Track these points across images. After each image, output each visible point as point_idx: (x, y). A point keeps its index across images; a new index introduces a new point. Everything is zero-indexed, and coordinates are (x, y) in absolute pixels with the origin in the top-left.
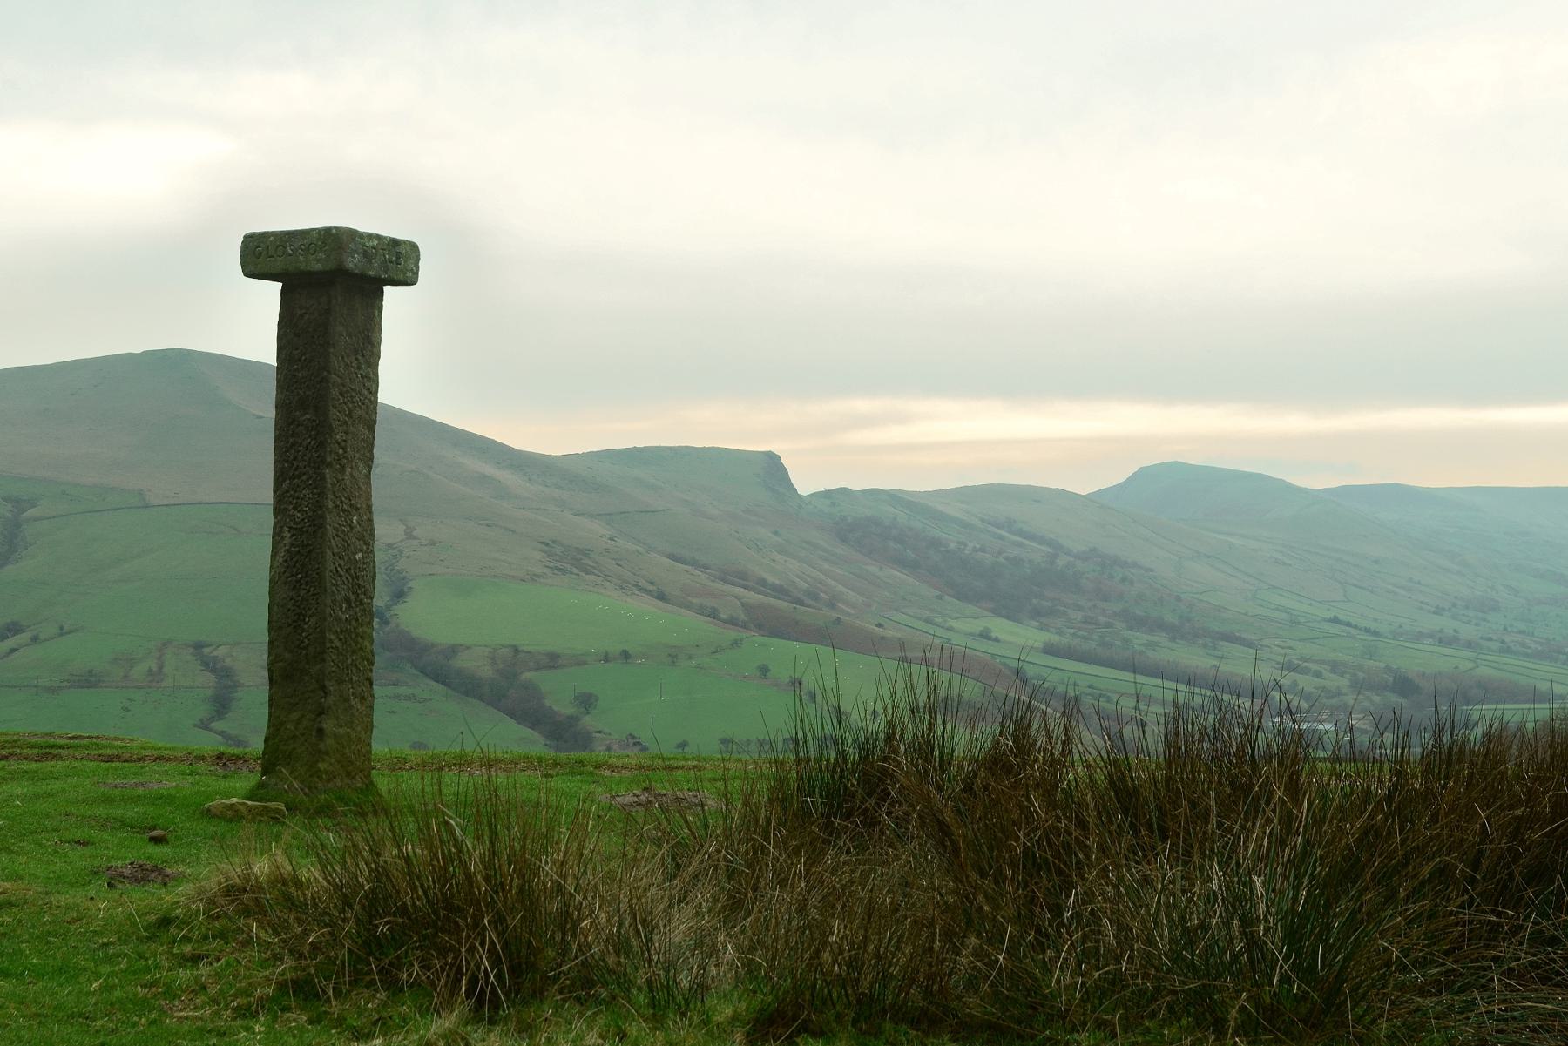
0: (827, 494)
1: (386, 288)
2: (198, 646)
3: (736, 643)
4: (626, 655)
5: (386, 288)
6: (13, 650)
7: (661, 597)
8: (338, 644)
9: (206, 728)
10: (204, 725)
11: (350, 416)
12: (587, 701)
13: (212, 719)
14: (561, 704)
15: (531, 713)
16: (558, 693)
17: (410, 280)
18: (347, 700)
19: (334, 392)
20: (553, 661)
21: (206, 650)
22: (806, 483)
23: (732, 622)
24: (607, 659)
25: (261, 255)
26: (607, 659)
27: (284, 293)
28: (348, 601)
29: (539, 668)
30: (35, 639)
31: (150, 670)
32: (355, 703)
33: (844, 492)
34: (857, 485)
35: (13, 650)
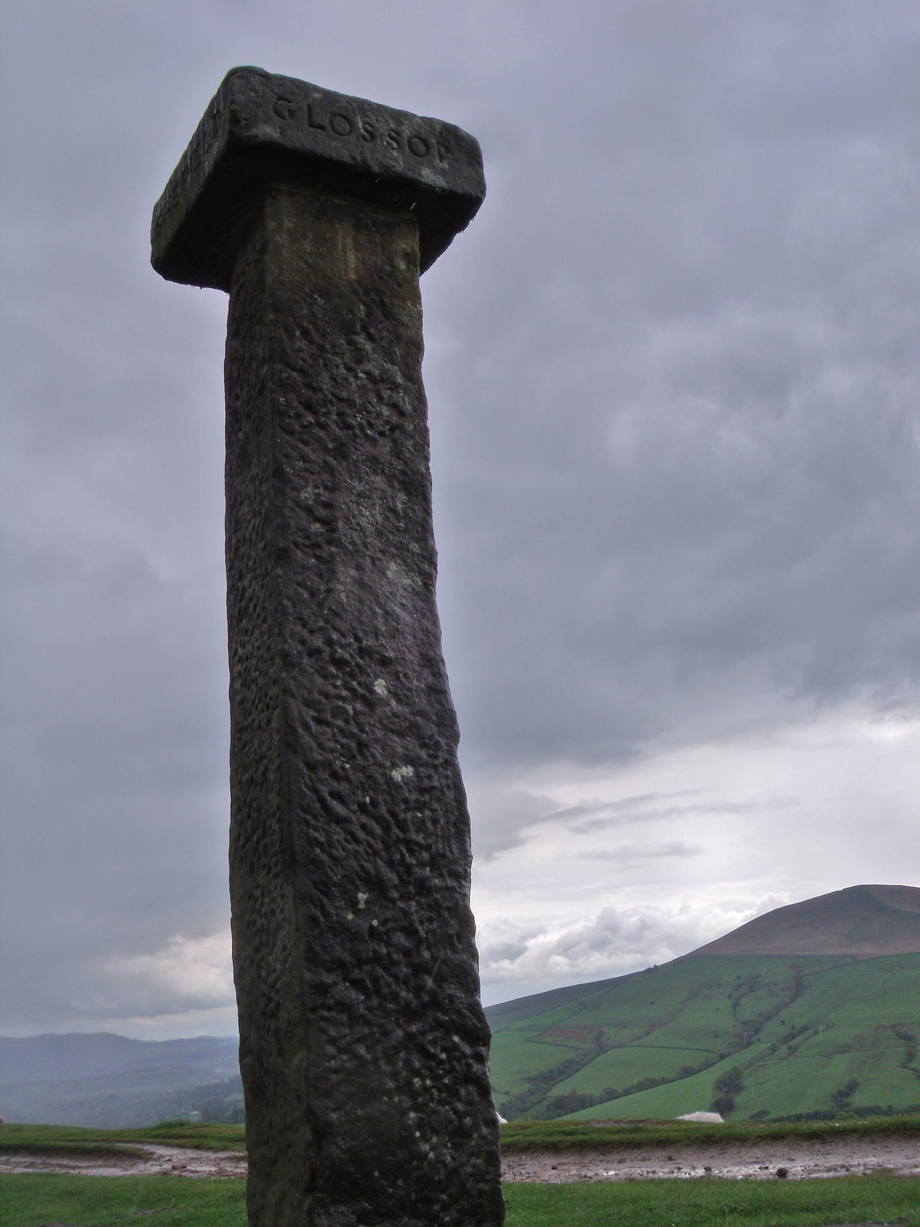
6: (807, 1039)
10: (903, 1066)
35: (807, 1039)
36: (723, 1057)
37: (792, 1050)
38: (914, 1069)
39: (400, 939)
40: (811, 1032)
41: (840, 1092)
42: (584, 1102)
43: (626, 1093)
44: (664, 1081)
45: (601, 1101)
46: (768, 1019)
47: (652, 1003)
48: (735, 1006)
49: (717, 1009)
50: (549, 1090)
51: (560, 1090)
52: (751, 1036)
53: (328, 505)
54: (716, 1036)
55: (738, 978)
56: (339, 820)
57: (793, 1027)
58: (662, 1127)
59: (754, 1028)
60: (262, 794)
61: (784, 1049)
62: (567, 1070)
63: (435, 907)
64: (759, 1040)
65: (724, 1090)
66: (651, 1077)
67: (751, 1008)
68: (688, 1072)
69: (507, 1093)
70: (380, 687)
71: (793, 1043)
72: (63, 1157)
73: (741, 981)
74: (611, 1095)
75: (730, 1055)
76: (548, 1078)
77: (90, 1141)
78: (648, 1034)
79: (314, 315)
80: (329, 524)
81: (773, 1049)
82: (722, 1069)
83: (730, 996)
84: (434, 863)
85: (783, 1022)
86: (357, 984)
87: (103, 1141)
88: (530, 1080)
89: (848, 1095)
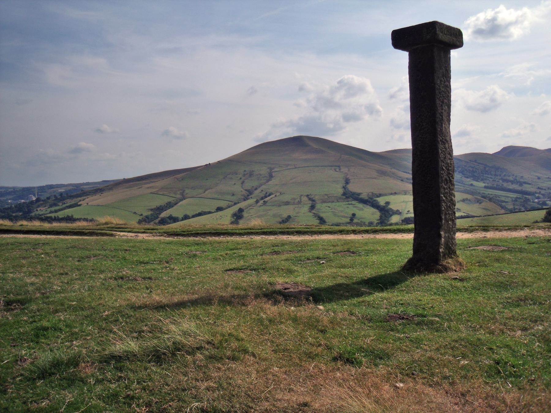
2: (307, 196)
12: (388, 203)
15: (375, 205)
16: (382, 201)
19: (437, 92)
25: (401, 38)
28: (446, 179)
30: (276, 196)
36: (235, 204)
38: (314, 213)
40: (273, 196)
42: (175, 220)
43: (194, 216)
44: (210, 213)
45: (183, 219)
46: (256, 189)
50: (160, 214)
51: (164, 215)
52: (248, 196)
54: (233, 195)
55: (245, 171)
57: (266, 193)
58: (290, 230)
59: (250, 192)
60: (477, 272)
61: (262, 202)
62: (170, 205)
66: (204, 211)
67: (249, 184)
68: (219, 209)
69: (142, 215)
71: (266, 199)
72: (34, 234)
73: (246, 173)
74: (186, 217)
75: (239, 203)
76: (160, 209)
77: (87, 229)
78: (204, 192)
80: (442, 116)
81: (257, 202)
82: (235, 208)
83: (241, 178)
87: (250, 229)
88: (152, 210)
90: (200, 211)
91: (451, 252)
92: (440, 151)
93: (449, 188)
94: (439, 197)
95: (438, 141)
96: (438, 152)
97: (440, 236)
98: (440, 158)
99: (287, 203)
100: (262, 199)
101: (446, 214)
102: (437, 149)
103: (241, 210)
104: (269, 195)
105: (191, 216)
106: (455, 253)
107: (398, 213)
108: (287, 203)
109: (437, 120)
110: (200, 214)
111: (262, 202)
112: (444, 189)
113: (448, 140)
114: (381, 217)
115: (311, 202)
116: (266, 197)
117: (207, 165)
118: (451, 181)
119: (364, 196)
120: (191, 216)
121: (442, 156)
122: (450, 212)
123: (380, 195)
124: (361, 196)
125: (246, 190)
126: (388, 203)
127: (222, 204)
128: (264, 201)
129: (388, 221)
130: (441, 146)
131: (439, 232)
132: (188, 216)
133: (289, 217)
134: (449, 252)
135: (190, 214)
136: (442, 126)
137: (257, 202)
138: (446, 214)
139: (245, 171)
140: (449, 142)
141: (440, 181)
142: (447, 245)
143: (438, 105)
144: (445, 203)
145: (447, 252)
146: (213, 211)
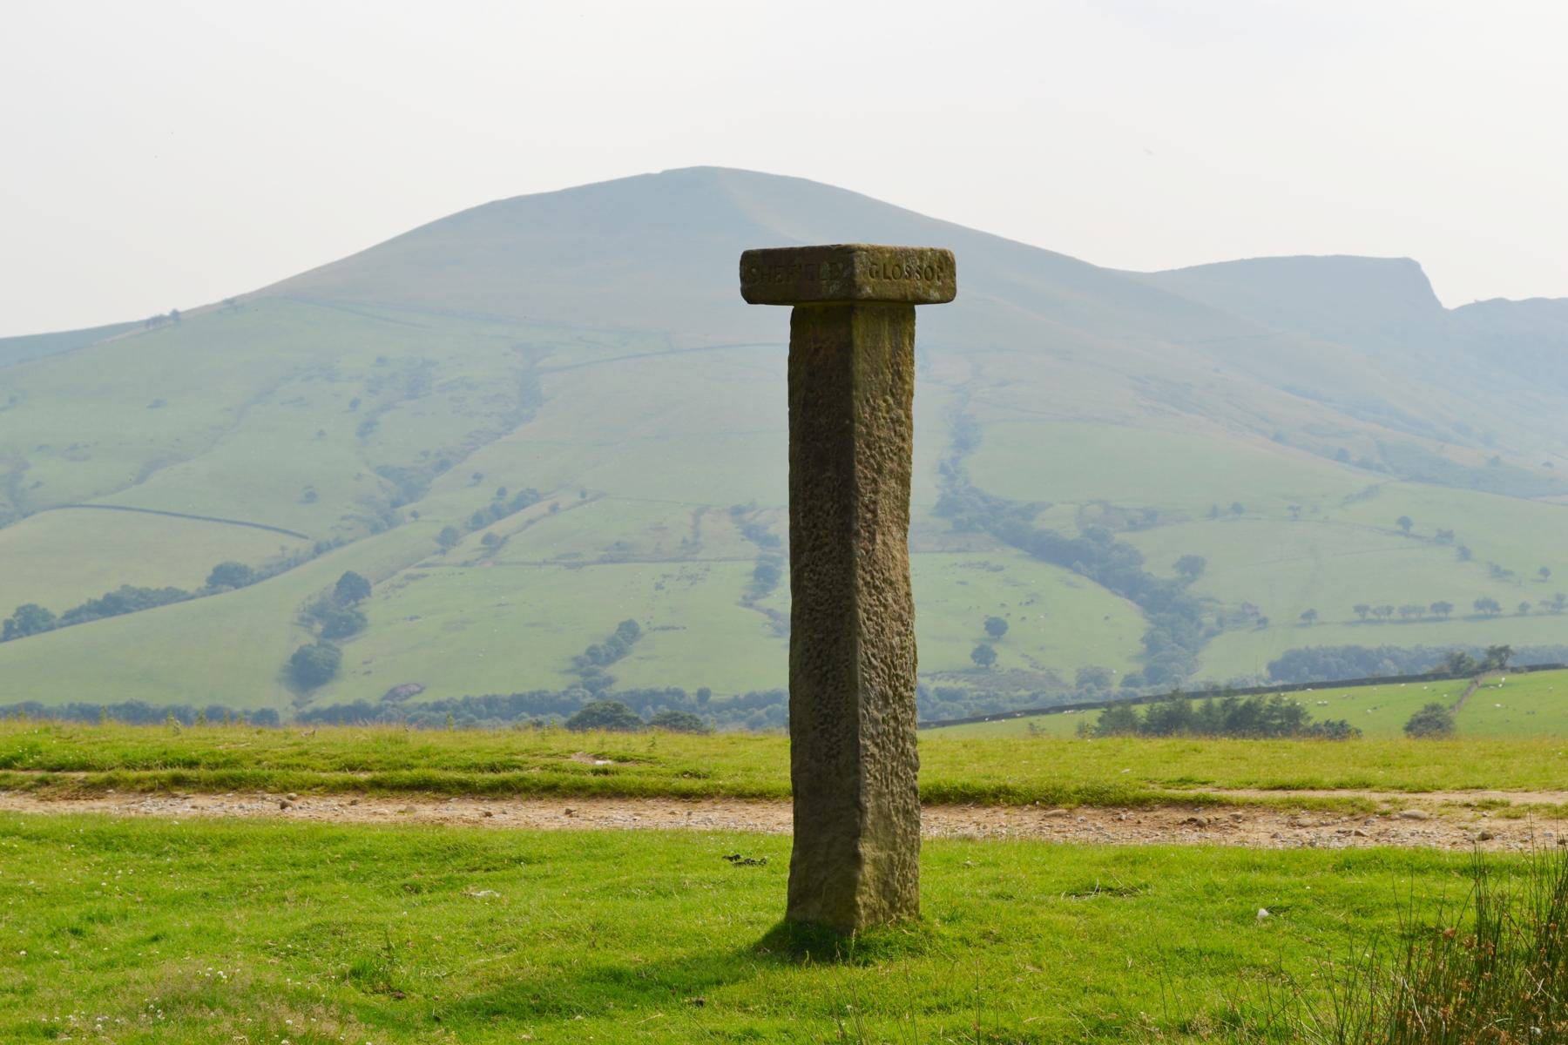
0: (1478, 307)
1: (917, 307)
2: (737, 511)
3: (1369, 493)
4: (1237, 509)
5: (917, 307)
6: (531, 522)
7: (1278, 438)
8: (876, 751)
9: (750, 605)
10: (748, 603)
11: (879, 471)
12: (1192, 566)
13: (755, 598)
14: (1160, 569)
15: (1121, 577)
16: (1158, 556)
17: (948, 296)
18: (889, 817)
19: (859, 444)
20: (1150, 519)
21: (747, 516)
22: (1452, 292)
23: (1365, 465)
24: (1214, 513)
25: (766, 275)
26: (1185, 1029)
27: (795, 321)
28: (884, 697)
29: (1134, 526)
30: (554, 509)
31: (684, 541)
32: (898, 820)
33: (1499, 303)
34: (1516, 293)
35: (531, 522)
36: (319, 550)
37: (493, 545)
39: (892, 723)
41: (593, 653)
43: (73, 617)
46: (443, 466)
47: (157, 404)
48: (367, 428)
49: (321, 433)
52: (396, 504)
53: (875, 502)
54: (311, 497)
55: (381, 361)
56: (875, 668)
57: (502, 492)
61: (474, 539)
63: (904, 706)
64: (415, 514)
65: (318, 627)
66: (138, 584)
70: (890, 597)
71: (498, 528)
78: (141, 479)
79: (1307, 985)
80: (874, 512)
81: (448, 538)
82: (320, 577)
83: (354, 404)
84: (905, 686)
85: (478, 477)
86: (877, 745)
89: (610, 660)
90: (112, 586)
91: (896, 898)
92: (862, 615)
93: (896, 718)
94: (856, 746)
95: (857, 588)
96: (854, 617)
97: (857, 859)
98: (860, 634)
99: (619, 554)
100: (478, 522)
101: (879, 795)
102: (851, 609)
103: (353, 587)
104: (519, 505)
105: (58, 613)
106: (916, 907)
107: (1251, 618)
108: (619, 554)
109: (856, 526)
110: (111, 606)
111: (474, 539)
112: (875, 722)
113: (895, 575)
114: (1152, 644)
115: (752, 548)
116: (498, 513)
117: (157, 321)
118: (902, 698)
119: (1061, 523)
120: (58, 613)
121: (867, 629)
122: (896, 789)
123: (1150, 519)
124: (1041, 523)
125: (383, 471)
126: (1192, 566)
127: (252, 549)
128: (487, 540)
129: (1189, 672)
130: (864, 600)
131: (856, 847)
132: (46, 616)
133: (629, 631)
134: (892, 906)
135: (56, 602)
136: (873, 540)
137: (448, 538)
138: (879, 795)
139: (381, 361)
140: (901, 585)
141: (861, 700)
142: (886, 884)
143: (860, 483)
144: (876, 762)
145: (885, 904)
146: (190, 586)
